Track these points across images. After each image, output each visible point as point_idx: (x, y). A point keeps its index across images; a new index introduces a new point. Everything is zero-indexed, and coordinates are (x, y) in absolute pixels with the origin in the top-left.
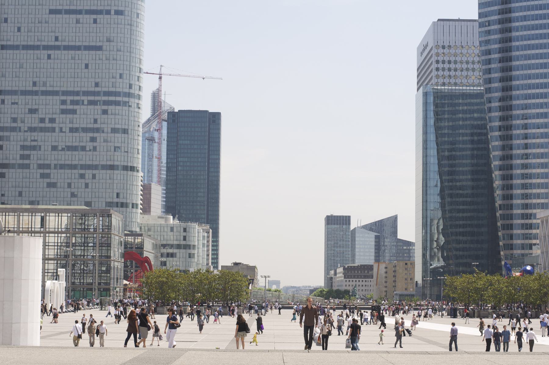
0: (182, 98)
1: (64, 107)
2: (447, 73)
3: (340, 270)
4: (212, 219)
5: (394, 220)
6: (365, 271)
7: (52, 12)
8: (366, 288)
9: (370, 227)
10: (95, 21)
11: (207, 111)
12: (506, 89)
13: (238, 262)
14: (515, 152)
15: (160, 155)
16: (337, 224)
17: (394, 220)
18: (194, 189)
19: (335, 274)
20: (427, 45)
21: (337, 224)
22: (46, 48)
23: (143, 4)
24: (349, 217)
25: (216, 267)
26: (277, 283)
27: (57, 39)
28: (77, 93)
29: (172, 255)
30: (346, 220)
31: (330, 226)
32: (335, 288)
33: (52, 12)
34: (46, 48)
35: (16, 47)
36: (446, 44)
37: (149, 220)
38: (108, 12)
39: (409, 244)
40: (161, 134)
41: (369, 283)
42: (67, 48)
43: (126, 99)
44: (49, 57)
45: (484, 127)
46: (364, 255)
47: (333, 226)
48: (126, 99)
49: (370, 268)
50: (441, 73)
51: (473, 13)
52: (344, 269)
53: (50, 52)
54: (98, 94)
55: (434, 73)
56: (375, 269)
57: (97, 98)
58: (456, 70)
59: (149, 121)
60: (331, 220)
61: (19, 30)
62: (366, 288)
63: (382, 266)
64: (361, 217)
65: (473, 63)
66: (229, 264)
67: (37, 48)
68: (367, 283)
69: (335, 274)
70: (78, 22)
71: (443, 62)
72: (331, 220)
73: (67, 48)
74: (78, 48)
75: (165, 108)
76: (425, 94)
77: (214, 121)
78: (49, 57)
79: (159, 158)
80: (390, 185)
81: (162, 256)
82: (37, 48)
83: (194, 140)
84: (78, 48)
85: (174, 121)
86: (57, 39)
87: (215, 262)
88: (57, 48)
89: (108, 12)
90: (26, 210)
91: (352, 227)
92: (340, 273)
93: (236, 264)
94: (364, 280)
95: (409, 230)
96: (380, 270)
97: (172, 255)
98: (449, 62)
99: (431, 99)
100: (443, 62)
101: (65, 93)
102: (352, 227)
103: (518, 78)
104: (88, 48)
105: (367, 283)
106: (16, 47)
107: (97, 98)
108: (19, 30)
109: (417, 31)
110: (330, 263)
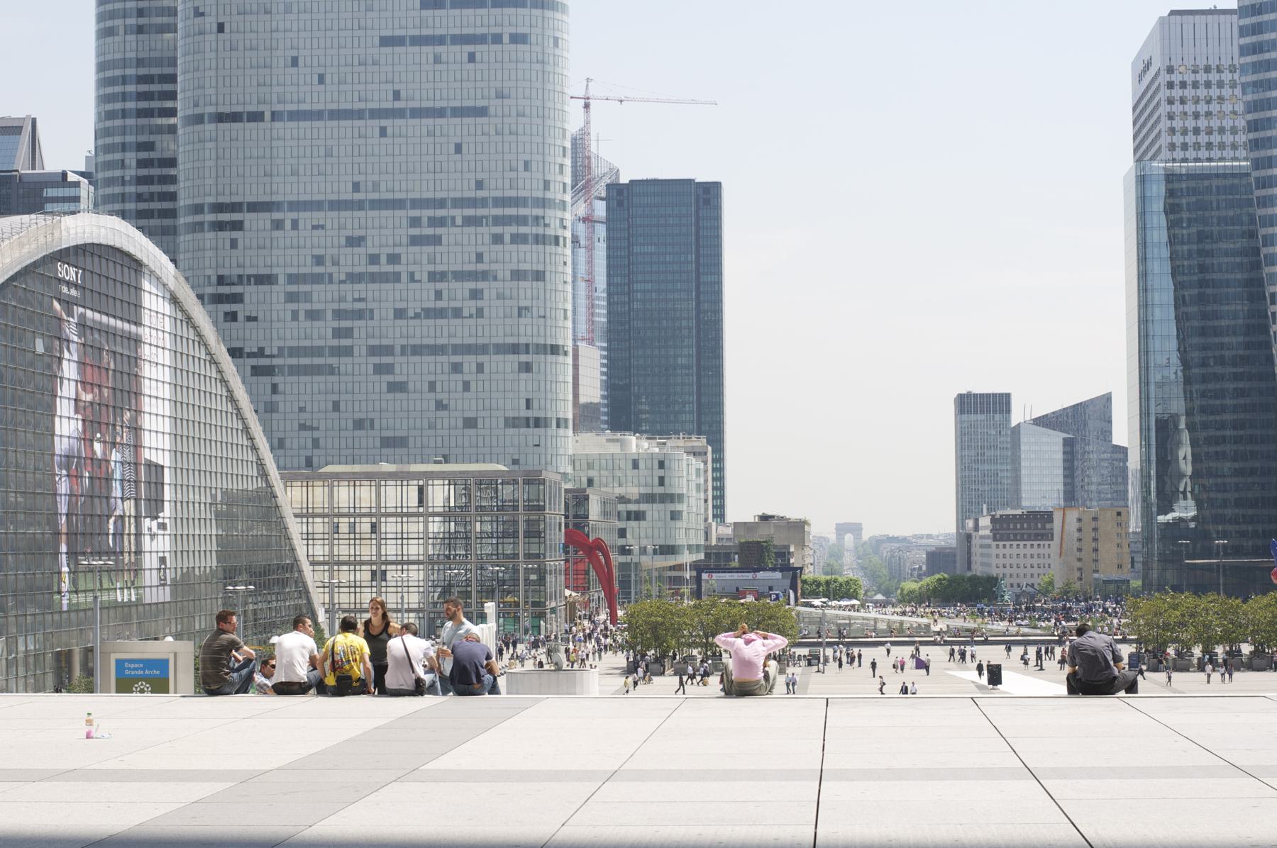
0: (635, 155)
3: (985, 522)
4: (708, 422)
5: (1107, 399)
6: (1034, 526)
7: (386, 41)
8: (1041, 561)
10: (472, 58)
11: (689, 182)
13: (769, 513)
15: (590, 272)
16: (981, 412)
17: (1107, 399)
18: (668, 356)
19: (976, 528)
21: (981, 412)
24: (716, 186)
25: (720, 514)
26: (856, 529)
28: (441, 203)
30: (1001, 403)
31: (965, 417)
33: (386, 41)
38: (497, 39)
39: (1124, 450)
41: (1046, 551)
42: (418, 113)
43: (538, 212)
44: (383, 132)
45: (1252, 235)
47: (973, 417)
48: (538, 212)
49: (1047, 517)
52: (993, 520)
54: (483, 202)
57: (481, 212)
60: (966, 404)
62: (1041, 561)
65: (1234, 131)
66: (750, 518)
68: (1041, 551)
69: (976, 528)
70: (437, 60)
72: (966, 404)
73: (418, 113)
74: (440, 113)
77: (707, 202)
78: (383, 132)
79: (590, 282)
80: (1080, 335)
83: (667, 247)
84: (440, 113)
85: (620, 204)
86: (397, 95)
89: (497, 39)
91: (1014, 423)
92: (985, 528)
93: (765, 518)
94: (1036, 543)
95: (1125, 430)
96: (1067, 523)
99: (1158, 190)
105: (1041, 551)
107: (481, 212)
108: (321, 79)
110: (967, 505)
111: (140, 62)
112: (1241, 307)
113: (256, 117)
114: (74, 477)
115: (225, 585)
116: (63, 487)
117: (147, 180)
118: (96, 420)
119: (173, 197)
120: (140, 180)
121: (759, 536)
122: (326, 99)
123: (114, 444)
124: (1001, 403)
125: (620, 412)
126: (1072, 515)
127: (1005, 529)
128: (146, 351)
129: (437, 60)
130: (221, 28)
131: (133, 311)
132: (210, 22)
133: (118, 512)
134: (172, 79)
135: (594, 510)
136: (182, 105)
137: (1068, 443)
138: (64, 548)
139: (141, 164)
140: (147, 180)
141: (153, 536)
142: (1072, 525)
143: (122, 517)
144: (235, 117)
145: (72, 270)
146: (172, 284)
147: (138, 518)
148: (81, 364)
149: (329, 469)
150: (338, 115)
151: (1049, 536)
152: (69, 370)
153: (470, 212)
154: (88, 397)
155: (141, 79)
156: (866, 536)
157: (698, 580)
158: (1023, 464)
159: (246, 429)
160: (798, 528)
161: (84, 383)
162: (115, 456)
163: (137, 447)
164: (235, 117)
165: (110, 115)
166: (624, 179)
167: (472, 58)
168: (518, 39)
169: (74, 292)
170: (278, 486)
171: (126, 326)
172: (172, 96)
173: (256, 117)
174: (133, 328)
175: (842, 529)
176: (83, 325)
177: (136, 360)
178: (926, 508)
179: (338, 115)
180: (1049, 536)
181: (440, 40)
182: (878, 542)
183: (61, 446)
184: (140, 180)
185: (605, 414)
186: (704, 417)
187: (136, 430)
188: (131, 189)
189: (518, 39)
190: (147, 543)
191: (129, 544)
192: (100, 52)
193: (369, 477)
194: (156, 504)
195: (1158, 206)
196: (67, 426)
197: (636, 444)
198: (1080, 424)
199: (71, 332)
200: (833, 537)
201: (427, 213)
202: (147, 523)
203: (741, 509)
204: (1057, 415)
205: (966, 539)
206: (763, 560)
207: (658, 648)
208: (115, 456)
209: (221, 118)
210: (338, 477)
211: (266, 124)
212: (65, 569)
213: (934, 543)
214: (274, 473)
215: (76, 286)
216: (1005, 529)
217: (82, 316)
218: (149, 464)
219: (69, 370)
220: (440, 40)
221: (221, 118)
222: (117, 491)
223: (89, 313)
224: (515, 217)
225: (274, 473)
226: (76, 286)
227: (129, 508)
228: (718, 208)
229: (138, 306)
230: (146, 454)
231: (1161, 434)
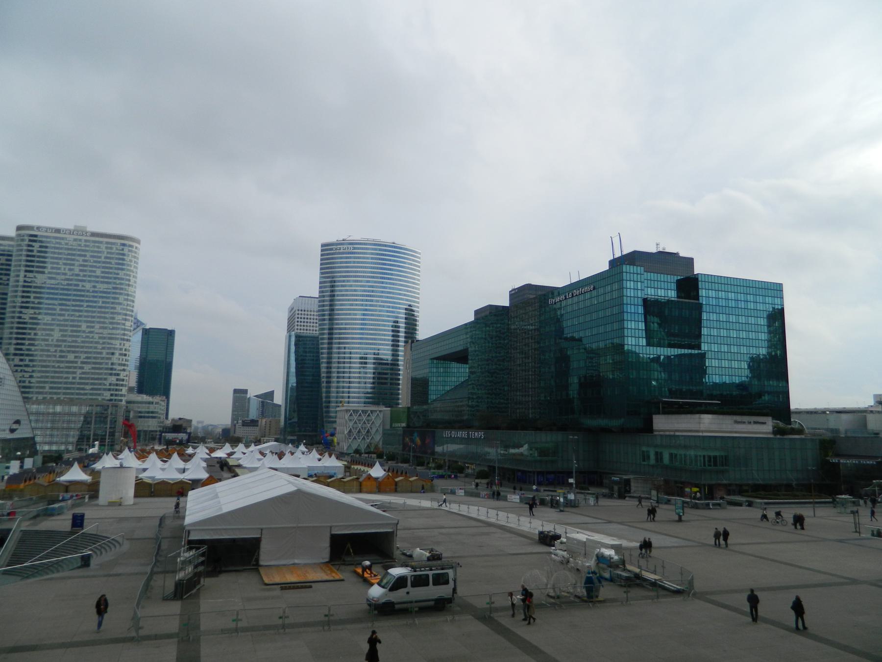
0: (154, 319)
4: (168, 397)
5: (272, 393)
6: (254, 423)
12: (331, 301)
16: (240, 395)
17: (272, 393)
18: (155, 374)
21: (240, 395)
23: (194, 423)
24: (692, 259)
25: (167, 418)
26: (202, 422)
30: (245, 392)
32: (325, 424)
39: (280, 406)
45: (318, 352)
46: (253, 413)
51: (316, 293)
63: (264, 421)
64: (255, 390)
66: (177, 417)
76: (290, 336)
80: (270, 374)
93: (180, 419)
95: (279, 399)
96: (263, 422)
99: (293, 339)
103: (338, 286)
110: (235, 418)
115: (589, 506)
121: (179, 423)
124: (245, 392)
125: (141, 388)
126: (264, 421)
127: (245, 424)
135: (132, 415)
138: (512, 451)
157: (161, 435)
160: (190, 421)
166: (147, 327)
175: (198, 422)
185: (323, 358)
186: (165, 390)
195: (293, 343)
197: (145, 398)
204: (262, 394)
211: (95, 617)
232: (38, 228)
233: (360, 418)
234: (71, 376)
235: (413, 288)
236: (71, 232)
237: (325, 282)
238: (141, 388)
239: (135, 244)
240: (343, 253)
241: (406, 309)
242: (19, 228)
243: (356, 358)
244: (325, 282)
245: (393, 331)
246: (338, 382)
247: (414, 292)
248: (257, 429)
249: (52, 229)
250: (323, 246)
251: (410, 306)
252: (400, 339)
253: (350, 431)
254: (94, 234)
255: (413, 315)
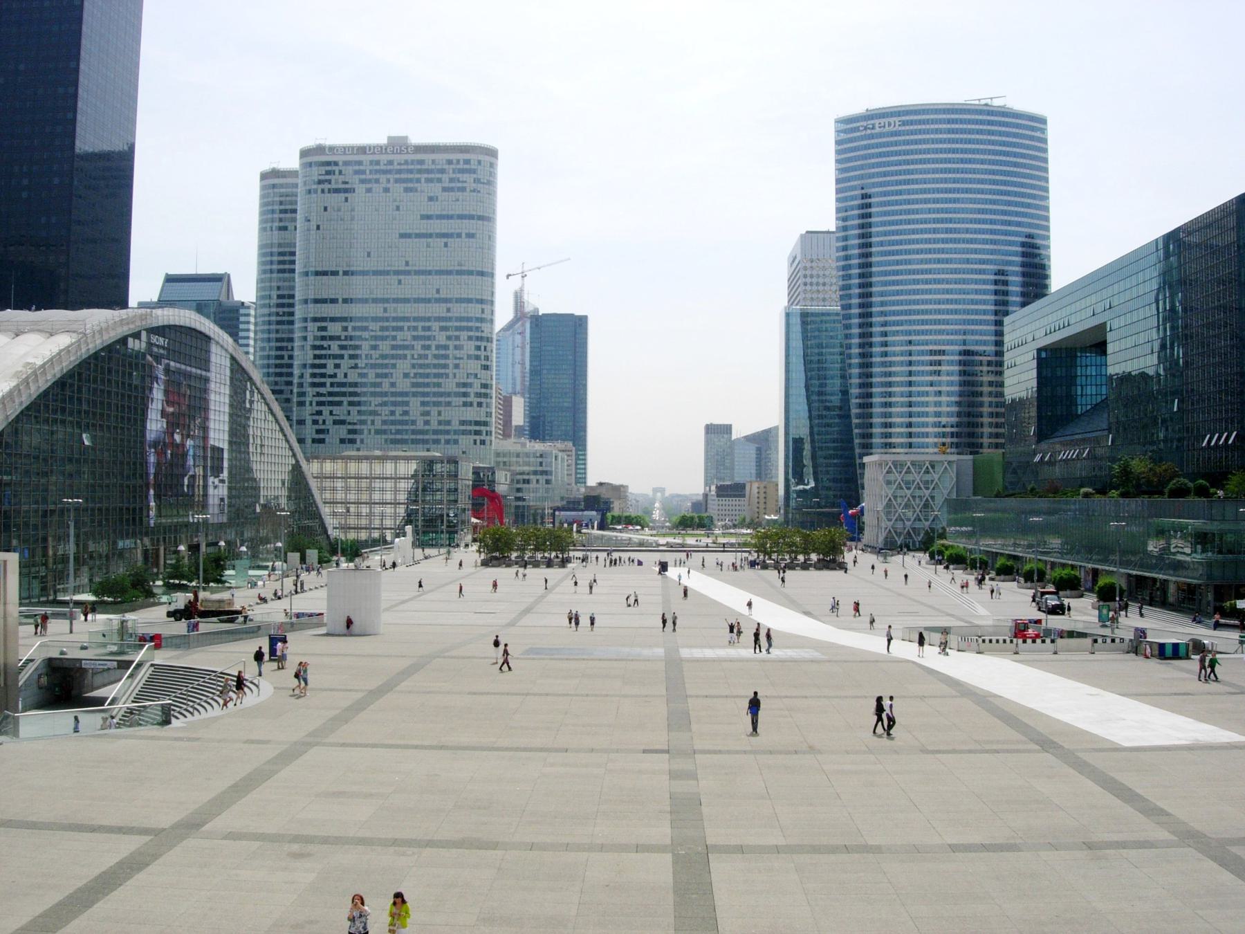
0: (549, 300)
1: (415, 333)
2: (815, 288)
3: (713, 488)
7: (402, 236)
9: (751, 439)
10: (446, 245)
11: (572, 315)
14: (874, 380)
15: (523, 360)
17: (776, 428)
20: (795, 258)
22: (397, 273)
26: (662, 490)
27: (407, 264)
28: (429, 319)
29: (528, 482)
30: (727, 429)
33: (402, 236)
34: (397, 273)
35: (364, 273)
36: (814, 257)
37: (506, 452)
38: (459, 235)
40: (524, 337)
42: (418, 273)
43: (478, 324)
44: (400, 282)
48: (478, 324)
49: (743, 487)
50: (808, 287)
53: (401, 277)
54: (450, 319)
55: (802, 288)
56: (748, 488)
57: (449, 324)
58: (824, 284)
59: (511, 326)
60: (711, 430)
61: (369, 255)
67: (387, 273)
70: (428, 246)
71: (812, 276)
72: (711, 430)
73: (418, 273)
74: (430, 273)
75: (528, 309)
78: (400, 282)
79: (523, 364)
80: (759, 399)
81: (518, 482)
82: (387, 273)
83: (559, 346)
84: (430, 273)
86: (407, 264)
87: (581, 478)
88: (408, 273)
89: (459, 235)
90: (377, 458)
91: (734, 437)
93: (601, 484)
97: (528, 482)
98: (818, 276)
100: (812, 276)
101: (416, 319)
102: (734, 437)
104: (440, 272)
106: (364, 273)
107: (449, 324)
108: (369, 255)
109: (788, 244)
111: (280, 245)
112: (838, 382)
113: (335, 273)
114: (161, 454)
116: (152, 459)
117: (282, 305)
118: (173, 422)
119: (292, 314)
120: (279, 305)
122: (370, 265)
123: (188, 436)
124: (727, 429)
128: (212, 386)
129: (428, 246)
130: (318, 227)
131: (205, 364)
132: (313, 225)
133: (191, 473)
134: (293, 254)
136: (298, 267)
137: (759, 449)
138: (152, 492)
139: (279, 297)
140: (282, 305)
141: (215, 487)
142: (755, 490)
143: (193, 477)
144: (325, 273)
145: (161, 339)
146: (231, 350)
147: (205, 477)
148: (166, 392)
149: (346, 453)
150: (376, 273)
151: (744, 496)
152: (158, 394)
153: (444, 324)
154: (171, 410)
155: (280, 254)
156: (667, 494)
157: (553, 515)
158: (227, 418)
159: (282, 430)
161: (168, 402)
162: (189, 443)
163: (205, 438)
164: (325, 273)
165: (264, 272)
167: (446, 245)
168: (471, 236)
169: (162, 351)
170: (303, 464)
171: (199, 372)
172: (293, 262)
173: (335, 273)
174: (204, 373)
175: (655, 490)
176: (167, 370)
177: (206, 391)
178: (690, 481)
179: (376, 273)
180: (744, 496)
181: (430, 236)
182: (673, 496)
183: (150, 436)
184: (279, 305)
186: (576, 435)
187: (205, 429)
188: (274, 310)
189: (471, 236)
190: (211, 491)
191: (199, 491)
192: (260, 240)
193: (367, 458)
194: (217, 470)
196: (155, 425)
198: (762, 440)
199: (160, 371)
200: (650, 493)
201: (421, 324)
202: (211, 479)
203: (592, 481)
205: (706, 496)
206: (602, 506)
207: (497, 552)
208: (189, 443)
209: (317, 273)
210: (350, 458)
211: (340, 277)
212: (152, 504)
213: (695, 499)
214: (300, 456)
215: (163, 348)
216: (723, 491)
217: (168, 365)
218: (214, 448)
219: (158, 394)
220: (430, 236)
221: (317, 273)
222: (190, 462)
223: (172, 364)
224: (475, 326)
225: (300, 456)
226: (163, 348)
227: (199, 471)
228: (586, 329)
229: (208, 361)
230: (212, 442)
231: (796, 447)
232: (332, 149)
233: (909, 478)
234: (399, 410)
235: (1029, 206)
236: (381, 149)
237: (848, 179)
238: (537, 429)
239: (487, 158)
240: (881, 135)
241: (1023, 245)
242: (304, 153)
243: (923, 363)
244: (848, 179)
245: (996, 293)
246: (885, 334)
247: (1034, 197)
248: (743, 502)
249: (353, 148)
250: (838, 121)
251: (1030, 236)
252: (1018, 289)
253: (889, 505)
254: (420, 149)
255: (1036, 256)
